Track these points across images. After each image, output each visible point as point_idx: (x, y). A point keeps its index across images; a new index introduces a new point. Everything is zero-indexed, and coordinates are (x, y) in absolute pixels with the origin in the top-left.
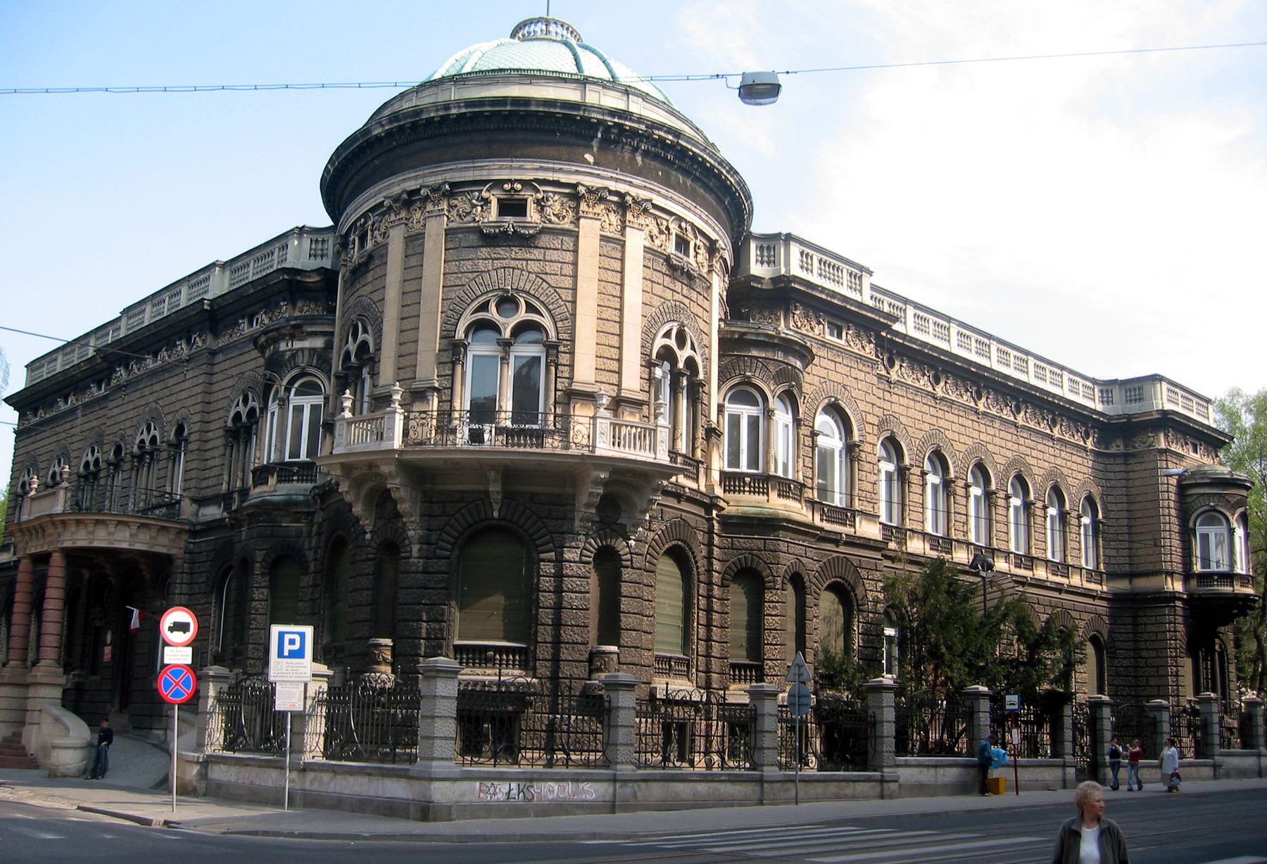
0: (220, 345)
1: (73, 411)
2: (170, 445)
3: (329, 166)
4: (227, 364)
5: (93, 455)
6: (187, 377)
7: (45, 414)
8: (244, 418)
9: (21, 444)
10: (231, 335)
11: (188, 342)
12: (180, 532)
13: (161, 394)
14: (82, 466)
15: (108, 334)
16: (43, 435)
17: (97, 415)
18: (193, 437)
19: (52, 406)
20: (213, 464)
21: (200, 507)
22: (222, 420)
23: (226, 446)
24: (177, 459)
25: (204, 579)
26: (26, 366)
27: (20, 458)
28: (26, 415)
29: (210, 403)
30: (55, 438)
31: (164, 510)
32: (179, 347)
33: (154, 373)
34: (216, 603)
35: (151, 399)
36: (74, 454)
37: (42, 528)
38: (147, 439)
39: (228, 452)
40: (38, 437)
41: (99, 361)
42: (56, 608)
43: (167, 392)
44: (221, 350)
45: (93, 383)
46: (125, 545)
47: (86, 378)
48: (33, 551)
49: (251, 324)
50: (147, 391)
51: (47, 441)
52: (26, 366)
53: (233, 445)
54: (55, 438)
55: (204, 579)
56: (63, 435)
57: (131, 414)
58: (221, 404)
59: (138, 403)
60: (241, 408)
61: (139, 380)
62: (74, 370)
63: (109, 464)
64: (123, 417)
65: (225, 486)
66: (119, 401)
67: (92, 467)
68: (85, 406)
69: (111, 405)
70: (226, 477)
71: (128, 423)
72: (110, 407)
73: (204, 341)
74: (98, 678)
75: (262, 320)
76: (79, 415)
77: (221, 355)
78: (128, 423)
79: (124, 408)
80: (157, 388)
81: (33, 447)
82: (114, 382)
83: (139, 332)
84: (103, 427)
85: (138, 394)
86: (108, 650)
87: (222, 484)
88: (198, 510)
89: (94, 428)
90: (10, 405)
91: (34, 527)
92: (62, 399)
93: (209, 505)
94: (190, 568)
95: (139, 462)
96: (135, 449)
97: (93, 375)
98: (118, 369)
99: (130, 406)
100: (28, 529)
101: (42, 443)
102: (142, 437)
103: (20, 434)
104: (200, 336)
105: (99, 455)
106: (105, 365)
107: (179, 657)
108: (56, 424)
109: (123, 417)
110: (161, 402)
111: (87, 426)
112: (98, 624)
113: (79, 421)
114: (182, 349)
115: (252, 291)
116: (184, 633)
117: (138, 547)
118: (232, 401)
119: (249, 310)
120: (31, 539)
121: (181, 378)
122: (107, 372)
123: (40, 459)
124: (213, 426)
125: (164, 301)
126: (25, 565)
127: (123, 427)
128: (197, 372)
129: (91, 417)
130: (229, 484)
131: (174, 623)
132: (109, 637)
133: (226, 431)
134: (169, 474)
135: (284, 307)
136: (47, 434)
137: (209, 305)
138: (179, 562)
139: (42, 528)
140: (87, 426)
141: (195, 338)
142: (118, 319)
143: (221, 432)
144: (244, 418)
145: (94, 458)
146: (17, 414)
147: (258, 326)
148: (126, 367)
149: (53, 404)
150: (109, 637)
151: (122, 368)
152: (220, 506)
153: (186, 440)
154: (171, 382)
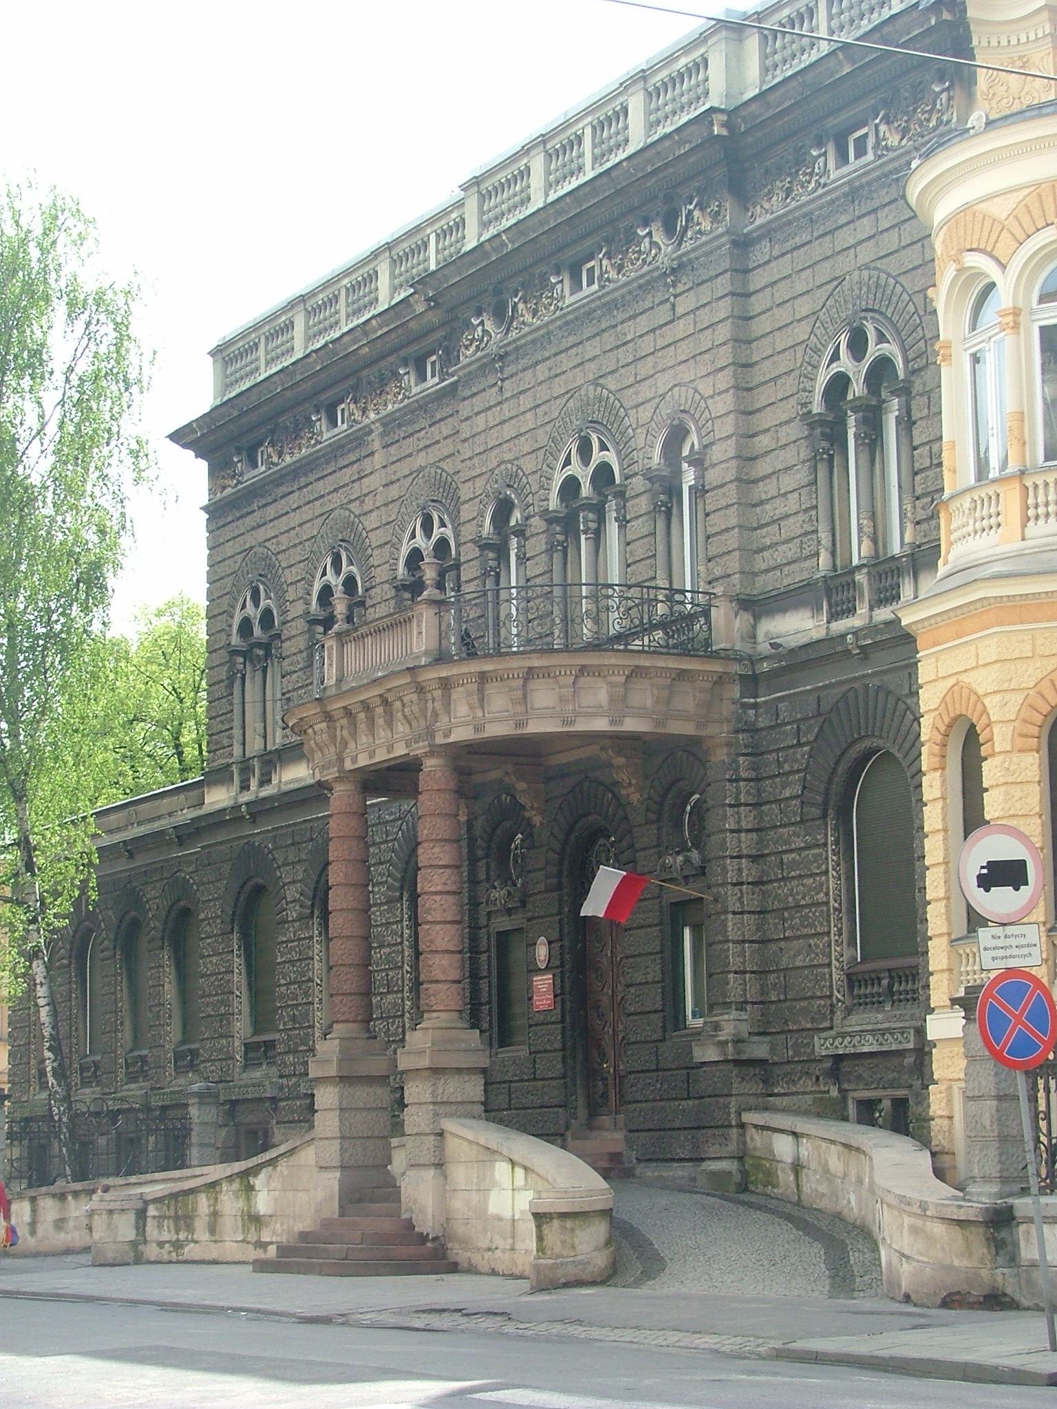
0: (758, 222)
1: (358, 440)
2: (484, 546)
3: (636, 103)
4: (782, 267)
5: (257, 605)
6: (680, 310)
7: (280, 455)
8: (857, 388)
9: (228, 532)
10: (789, 191)
11: (669, 230)
12: (721, 680)
13: (609, 363)
14: (235, 628)
15: (426, 245)
16: (281, 506)
17: (423, 439)
18: (717, 453)
19: (296, 433)
20: (781, 511)
21: (757, 618)
22: (793, 401)
23: (814, 460)
24: (675, 511)
25: (798, 789)
26: (213, 354)
27: (227, 567)
28: (228, 464)
29: (750, 365)
30: (318, 508)
31: (659, 635)
32: (646, 244)
33: (583, 316)
34: (836, 843)
35: (579, 378)
36: (375, 539)
37: (385, 702)
38: (584, 475)
39: (660, 525)
40: (271, 511)
41: (420, 308)
42: (448, 888)
43: (625, 355)
44: (768, 232)
45: (239, 452)
46: (600, 724)
47: (384, 356)
48: (363, 761)
49: (577, 285)
50: (566, 362)
51: (296, 518)
52: (213, 354)
53: (831, 457)
54: (318, 508)
55: (798, 789)
56: (337, 499)
57: (529, 421)
58: (784, 363)
59: (543, 393)
60: (576, 468)
61: (542, 339)
62: (355, 341)
63: (484, 546)
64: (509, 431)
65: (824, 559)
66: (492, 396)
67: (257, 631)
68: (390, 424)
69: (465, 409)
70: (824, 536)
71: (525, 445)
72: (465, 413)
73: (716, 217)
74: (522, 1052)
75: (878, 141)
76: (377, 445)
77: (765, 243)
78: (525, 445)
79: (507, 410)
80: (591, 349)
81: (261, 534)
82: (468, 355)
83: (535, 220)
84: (448, 466)
85: (542, 371)
86: (543, 984)
87: (817, 554)
88: (754, 627)
89: (421, 469)
90: (185, 446)
91: (366, 706)
92: (410, 369)
93: (783, 610)
94: (754, 767)
95: (565, 533)
96: (554, 503)
97: (402, 347)
98: (475, 322)
99: (526, 402)
100: (348, 713)
101: (283, 524)
102: (569, 471)
103: (218, 513)
104: (702, 207)
105: (448, 532)
106: (434, 317)
107: (1015, 951)
108: (312, 477)
109: (509, 431)
110: (611, 383)
111: (403, 468)
112: (502, 923)
113: (378, 459)
114: (653, 244)
115: (847, 69)
116: (1017, 889)
117: (631, 725)
118: (816, 351)
119: (569, 254)
120: (354, 735)
121: (663, 314)
122: (439, 335)
123: (370, 522)
124: (767, 419)
125: (580, 139)
126: (342, 795)
127: (507, 457)
128: (705, 294)
129: (408, 446)
130: (833, 554)
131: (990, 865)
132: (542, 952)
133: (811, 426)
134: (661, 548)
135: (944, 96)
136: (294, 500)
137: (725, 125)
138: (721, 755)
139: (385, 702)
140: (403, 468)
141: (515, 305)
142: (459, 204)
143: (795, 431)
144: (586, 490)
145: (342, 577)
146: (203, 466)
147: (595, 287)
148: (499, 314)
149: (299, 430)
150: (542, 952)
151: (485, 317)
152: (819, 609)
153: (621, 494)
154: (630, 330)
